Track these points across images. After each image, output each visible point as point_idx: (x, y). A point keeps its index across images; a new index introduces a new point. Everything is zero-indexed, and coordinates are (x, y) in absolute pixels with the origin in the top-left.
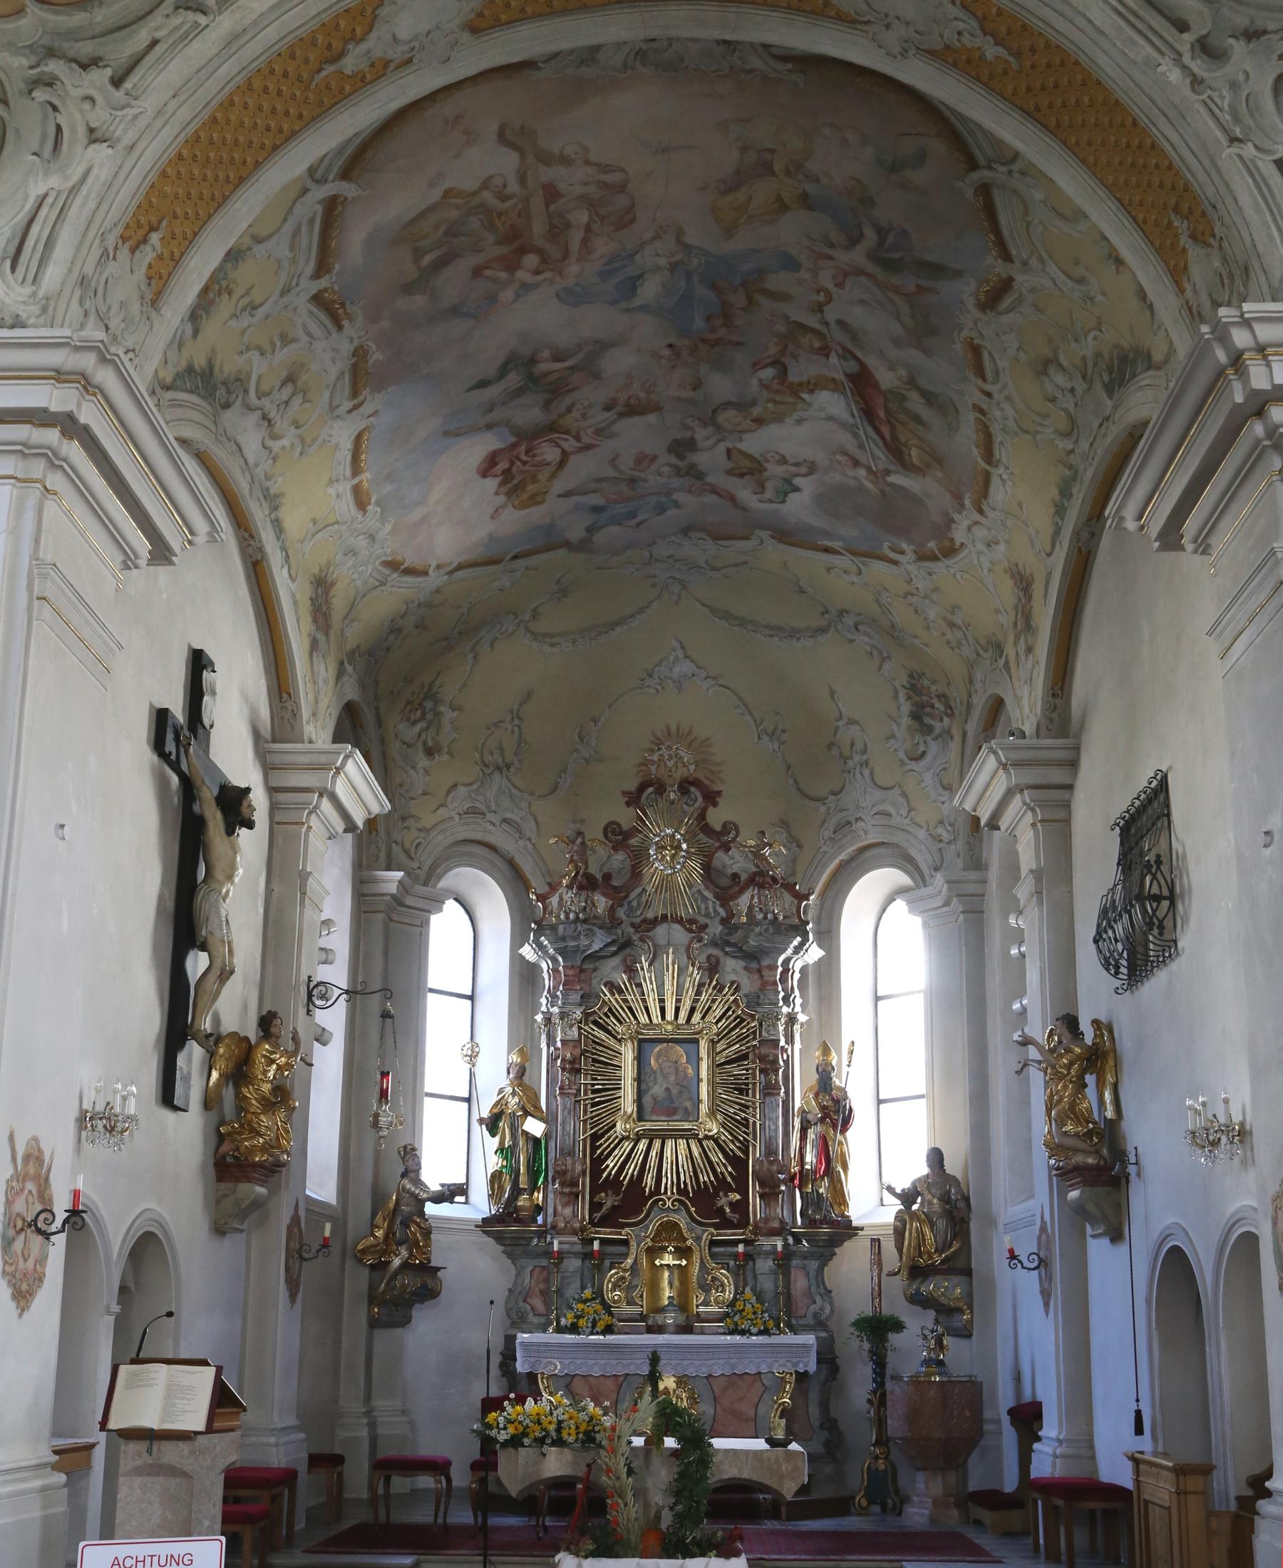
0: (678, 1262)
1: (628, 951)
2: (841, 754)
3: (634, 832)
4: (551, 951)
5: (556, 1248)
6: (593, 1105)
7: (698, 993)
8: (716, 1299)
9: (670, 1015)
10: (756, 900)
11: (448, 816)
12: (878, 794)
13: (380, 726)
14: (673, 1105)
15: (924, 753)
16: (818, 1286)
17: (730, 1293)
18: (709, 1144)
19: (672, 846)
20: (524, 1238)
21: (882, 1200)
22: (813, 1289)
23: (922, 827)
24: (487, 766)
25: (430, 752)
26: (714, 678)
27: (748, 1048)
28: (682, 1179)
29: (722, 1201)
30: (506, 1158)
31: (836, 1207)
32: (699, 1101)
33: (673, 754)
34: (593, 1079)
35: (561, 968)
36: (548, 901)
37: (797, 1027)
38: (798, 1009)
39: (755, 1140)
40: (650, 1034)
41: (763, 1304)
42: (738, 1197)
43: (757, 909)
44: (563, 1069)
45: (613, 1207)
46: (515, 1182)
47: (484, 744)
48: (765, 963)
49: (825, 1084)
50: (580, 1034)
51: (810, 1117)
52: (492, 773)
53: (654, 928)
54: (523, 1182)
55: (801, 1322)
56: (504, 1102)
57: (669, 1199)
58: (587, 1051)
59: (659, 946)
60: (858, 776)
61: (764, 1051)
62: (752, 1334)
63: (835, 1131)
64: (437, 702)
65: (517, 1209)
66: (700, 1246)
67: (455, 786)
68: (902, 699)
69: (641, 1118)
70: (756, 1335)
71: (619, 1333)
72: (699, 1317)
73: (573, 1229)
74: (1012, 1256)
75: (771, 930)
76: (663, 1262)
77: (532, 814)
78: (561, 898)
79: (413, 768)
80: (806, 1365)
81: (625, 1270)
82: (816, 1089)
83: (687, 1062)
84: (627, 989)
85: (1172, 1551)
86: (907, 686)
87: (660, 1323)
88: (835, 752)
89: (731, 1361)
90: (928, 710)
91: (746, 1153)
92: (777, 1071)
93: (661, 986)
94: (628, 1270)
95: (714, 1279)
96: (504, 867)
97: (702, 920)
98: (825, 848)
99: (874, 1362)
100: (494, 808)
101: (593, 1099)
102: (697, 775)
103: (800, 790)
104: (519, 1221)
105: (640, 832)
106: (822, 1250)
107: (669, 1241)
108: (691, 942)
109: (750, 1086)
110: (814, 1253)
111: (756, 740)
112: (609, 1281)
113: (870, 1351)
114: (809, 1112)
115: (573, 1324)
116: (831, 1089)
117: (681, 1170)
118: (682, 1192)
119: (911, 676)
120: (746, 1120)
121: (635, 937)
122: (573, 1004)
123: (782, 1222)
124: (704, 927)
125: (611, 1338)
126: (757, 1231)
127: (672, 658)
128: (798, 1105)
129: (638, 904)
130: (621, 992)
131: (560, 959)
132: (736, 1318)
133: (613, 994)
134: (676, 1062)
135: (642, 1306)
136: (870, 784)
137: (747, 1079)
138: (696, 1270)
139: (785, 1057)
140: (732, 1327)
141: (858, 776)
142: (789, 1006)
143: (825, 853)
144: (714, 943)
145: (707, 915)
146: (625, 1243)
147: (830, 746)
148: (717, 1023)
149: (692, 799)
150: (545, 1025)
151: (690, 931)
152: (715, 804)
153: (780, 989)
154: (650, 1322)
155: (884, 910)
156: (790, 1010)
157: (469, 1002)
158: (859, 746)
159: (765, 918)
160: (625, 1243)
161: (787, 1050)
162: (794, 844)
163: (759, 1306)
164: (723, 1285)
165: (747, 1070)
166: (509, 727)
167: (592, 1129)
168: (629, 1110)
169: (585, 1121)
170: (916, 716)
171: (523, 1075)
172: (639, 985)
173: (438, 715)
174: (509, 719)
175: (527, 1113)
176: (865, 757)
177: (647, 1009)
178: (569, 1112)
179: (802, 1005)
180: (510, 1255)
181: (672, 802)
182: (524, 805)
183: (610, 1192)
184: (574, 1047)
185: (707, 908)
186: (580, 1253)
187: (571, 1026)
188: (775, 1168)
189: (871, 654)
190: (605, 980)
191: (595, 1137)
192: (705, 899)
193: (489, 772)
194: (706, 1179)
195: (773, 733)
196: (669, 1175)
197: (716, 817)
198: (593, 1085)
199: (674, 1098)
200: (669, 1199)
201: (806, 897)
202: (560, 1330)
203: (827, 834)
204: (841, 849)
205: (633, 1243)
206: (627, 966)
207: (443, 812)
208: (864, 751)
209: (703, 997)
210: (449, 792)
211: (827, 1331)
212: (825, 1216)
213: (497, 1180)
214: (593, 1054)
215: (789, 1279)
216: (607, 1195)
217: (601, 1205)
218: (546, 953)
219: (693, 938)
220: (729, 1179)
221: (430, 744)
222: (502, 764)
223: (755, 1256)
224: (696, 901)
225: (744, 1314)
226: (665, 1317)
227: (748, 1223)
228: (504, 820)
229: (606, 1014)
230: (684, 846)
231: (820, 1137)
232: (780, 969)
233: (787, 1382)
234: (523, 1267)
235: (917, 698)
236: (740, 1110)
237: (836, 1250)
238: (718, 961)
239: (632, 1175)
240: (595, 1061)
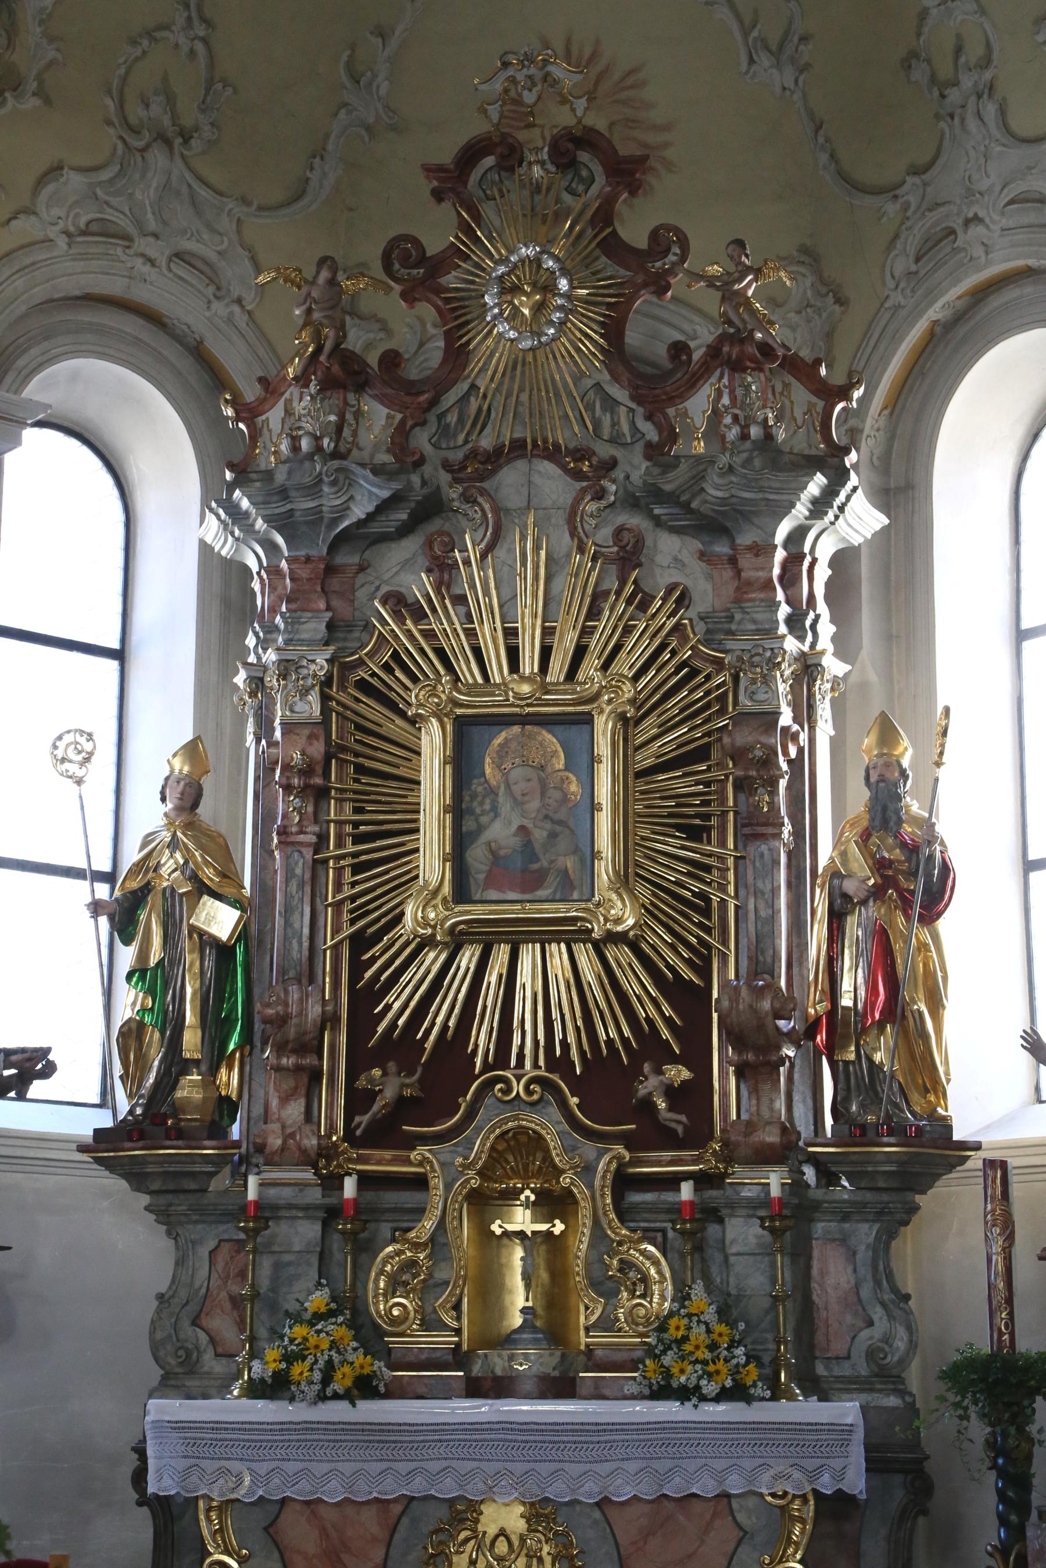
0: (543, 1227)
1: (436, 524)
2: (933, 79)
3: (453, 255)
4: (260, 524)
5: (252, 1195)
6: (357, 869)
7: (594, 613)
8: (630, 1313)
9: (529, 663)
10: (726, 400)
11: (39, 235)
12: (1016, 156)
14: (535, 866)
16: (878, 1283)
17: (663, 1298)
18: (620, 955)
19: (534, 285)
20: (193, 1175)
21: (1037, 1089)
22: (866, 1292)
24: (135, 131)
27: (708, 734)
28: (558, 1036)
29: (650, 1085)
30: (151, 991)
31: (915, 1097)
32: (595, 855)
33: (538, 75)
34: (358, 810)
35: (284, 564)
37: (823, 687)
38: (825, 643)
39: (725, 942)
40: (486, 704)
41: (732, 1324)
42: (686, 1074)
43: (728, 420)
44: (288, 788)
45: (401, 1101)
46: (174, 1044)
47: (124, 80)
48: (746, 538)
49: (885, 809)
50: (325, 711)
51: (850, 886)
52: (143, 150)
53: (494, 472)
54: (191, 1041)
55: (845, 1370)
56: (152, 863)
57: (519, 1078)
58: (344, 749)
59: (507, 511)
60: (972, 124)
61: (742, 737)
62: (704, 1399)
63: (908, 918)
65: (176, 1110)
66: (591, 1186)
69: (461, 893)
70: (717, 1399)
71: (388, 1395)
72: (591, 1359)
73: (304, 1152)
75: (757, 463)
76: (510, 1227)
77: (249, 248)
78: (288, 412)
80: (839, 1475)
81: (416, 1246)
82: (865, 823)
83: (567, 768)
84: (434, 610)
85: (880, 335)
87: (499, 1372)
89: (656, 1465)
91: (705, 972)
92: (773, 783)
93: (507, 604)
94: (424, 1245)
95: (626, 1265)
96: (186, 364)
97: (604, 451)
99: (1002, 1474)
100: (152, 225)
101: (355, 855)
102: (588, 121)
103: (843, 176)
104: (179, 1134)
105: (466, 258)
106: (885, 1197)
107: (526, 1177)
108: (577, 501)
109: (714, 822)
110: (864, 1205)
111: (744, 66)
112: (382, 1272)
113: (990, 1444)
114: (849, 876)
115: (276, 1374)
116: (900, 821)
117: (555, 1014)
118: (559, 1063)
120: (703, 896)
121: (453, 493)
122: (310, 643)
123: (788, 1130)
125: (371, 1410)
126: (729, 1156)
128: (823, 861)
129: (461, 421)
130: (419, 615)
131: (280, 540)
132: (668, 1359)
133: (400, 620)
134: (542, 768)
135: (458, 1332)
136: (996, 133)
137: (705, 803)
138: (581, 1245)
139: (793, 752)
140: (656, 1379)
142: (801, 639)
143: (898, 307)
144: (632, 502)
145: (615, 440)
146: (420, 1182)
147: (908, 62)
148: (636, 678)
149: (582, 180)
150: (253, 694)
151: (577, 475)
153: (780, 595)
154: (476, 1370)
155: (1036, 436)
156: (806, 648)
157: (114, 665)
158: (974, 52)
159: (744, 436)
160: (420, 1182)
161: (795, 737)
162: (830, 299)
163: (722, 1328)
164: (645, 1279)
165: (707, 784)
166: (182, 40)
167: (353, 922)
168: (434, 881)
169: (338, 905)
171: (195, 805)
172: (460, 600)
174: (180, 20)
175: (202, 889)
176: (987, 75)
177: (477, 652)
178: (301, 886)
179: (834, 639)
180: (163, 1215)
181: (537, 189)
182: (226, 224)
183: (392, 1066)
184: (311, 737)
185: (614, 424)
186: (317, 1207)
187: (305, 692)
188: (766, 1005)
190: (385, 589)
191: (360, 942)
192: (611, 404)
193: (141, 144)
194: (613, 1034)
195: (781, 46)
196: (528, 1026)
198: (356, 825)
199: (537, 847)
200: (519, 1078)
201: (844, 393)
202: (257, 1390)
203: (901, 265)
204: (931, 296)
205: (437, 1183)
206: (436, 558)
207: (25, 227)
208: (986, 62)
209: (604, 624)
210: (41, 182)
211: (902, 1393)
212: (889, 1117)
213: (133, 1045)
214: (357, 755)
215: (808, 1267)
216: (385, 1074)
217: (371, 1096)
218: (249, 529)
219: (584, 491)
220: (666, 1034)
222: (171, 132)
223: (724, 1212)
224: (590, 407)
225: (688, 1347)
226: (511, 1358)
227: (711, 1136)
228: (179, 255)
229: (387, 668)
230: (563, 284)
231: (874, 933)
232: (780, 555)
233: (793, 1520)
236: (689, 874)
237: (919, 1198)
238: (639, 542)
239: (445, 1027)
240: (360, 769)
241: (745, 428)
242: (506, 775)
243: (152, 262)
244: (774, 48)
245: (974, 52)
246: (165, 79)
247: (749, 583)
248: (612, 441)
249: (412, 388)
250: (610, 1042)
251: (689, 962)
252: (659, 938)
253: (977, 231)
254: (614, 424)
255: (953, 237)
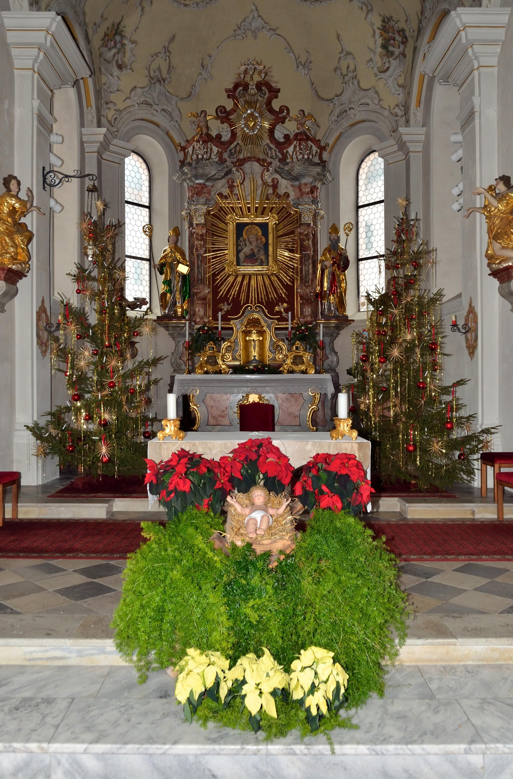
1: (230, 176)
2: (342, 74)
11: (132, 104)
12: (362, 93)
13: (89, 43)
15: (388, 68)
23: (386, 109)
25: (120, 67)
26: (274, 30)
34: (213, 244)
36: (186, 151)
52: (155, 83)
60: (351, 85)
64: (122, 37)
67: (135, 87)
68: (377, 36)
74: (455, 325)
78: (194, 148)
79: (111, 75)
86: (381, 27)
88: (338, 72)
90: (392, 42)
91: (293, 282)
97: (269, 160)
98: (332, 126)
100: (157, 102)
103: (318, 96)
119: (383, 21)
124: (270, 164)
127: (251, 17)
141: (351, 85)
143: (332, 129)
151: (263, 166)
152: (277, 97)
158: (352, 68)
159: (303, 158)
164: (282, 349)
166: (164, 56)
170: (384, 47)
173: (123, 45)
174: (163, 51)
182: (173, 102)
184: (203, 227)
185: (271, 153)
189: (362, 8)
192: (271, 149)
193: (153, 82)
195: (305, 64)
197: (276, 105)
207: (129, 102)
208: (355, 70)
210: (132, 91)
221: (120, 62)
222: (160, 79)
228: (163, 110)
234: (179, 342)
235: (386, 35)
239: (234, 294)
241: (303, 155)
242: (248, 236)
243: (157, 111)
244: (303, 64)
245: (352, 68)
246: (159, 66)
247: (304, 193)
248: (271, 158)
249: (223, 143)
250: (272, 298)
251: (290, 280)
252: (282, 275)
253: (352, 111)
254: (271, 153)
255: (13, 182)
